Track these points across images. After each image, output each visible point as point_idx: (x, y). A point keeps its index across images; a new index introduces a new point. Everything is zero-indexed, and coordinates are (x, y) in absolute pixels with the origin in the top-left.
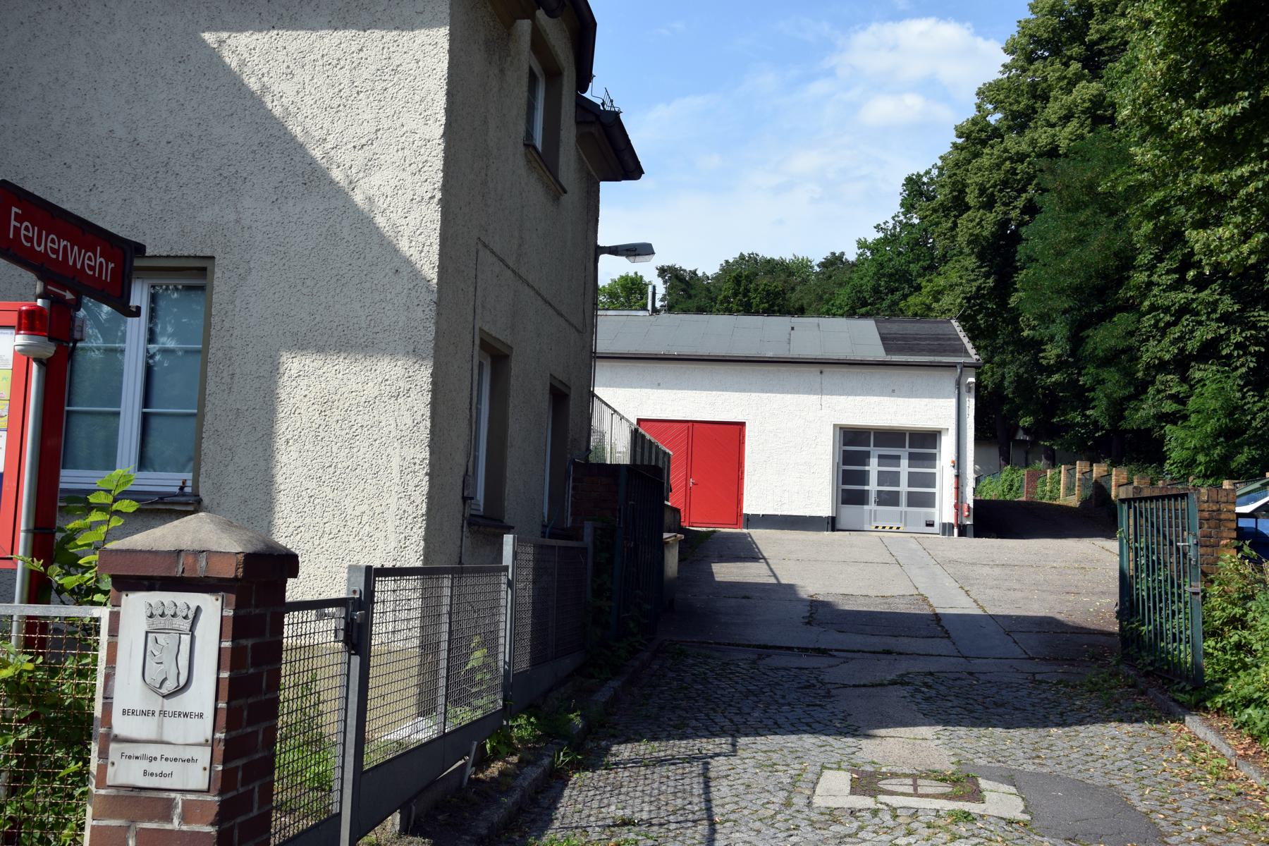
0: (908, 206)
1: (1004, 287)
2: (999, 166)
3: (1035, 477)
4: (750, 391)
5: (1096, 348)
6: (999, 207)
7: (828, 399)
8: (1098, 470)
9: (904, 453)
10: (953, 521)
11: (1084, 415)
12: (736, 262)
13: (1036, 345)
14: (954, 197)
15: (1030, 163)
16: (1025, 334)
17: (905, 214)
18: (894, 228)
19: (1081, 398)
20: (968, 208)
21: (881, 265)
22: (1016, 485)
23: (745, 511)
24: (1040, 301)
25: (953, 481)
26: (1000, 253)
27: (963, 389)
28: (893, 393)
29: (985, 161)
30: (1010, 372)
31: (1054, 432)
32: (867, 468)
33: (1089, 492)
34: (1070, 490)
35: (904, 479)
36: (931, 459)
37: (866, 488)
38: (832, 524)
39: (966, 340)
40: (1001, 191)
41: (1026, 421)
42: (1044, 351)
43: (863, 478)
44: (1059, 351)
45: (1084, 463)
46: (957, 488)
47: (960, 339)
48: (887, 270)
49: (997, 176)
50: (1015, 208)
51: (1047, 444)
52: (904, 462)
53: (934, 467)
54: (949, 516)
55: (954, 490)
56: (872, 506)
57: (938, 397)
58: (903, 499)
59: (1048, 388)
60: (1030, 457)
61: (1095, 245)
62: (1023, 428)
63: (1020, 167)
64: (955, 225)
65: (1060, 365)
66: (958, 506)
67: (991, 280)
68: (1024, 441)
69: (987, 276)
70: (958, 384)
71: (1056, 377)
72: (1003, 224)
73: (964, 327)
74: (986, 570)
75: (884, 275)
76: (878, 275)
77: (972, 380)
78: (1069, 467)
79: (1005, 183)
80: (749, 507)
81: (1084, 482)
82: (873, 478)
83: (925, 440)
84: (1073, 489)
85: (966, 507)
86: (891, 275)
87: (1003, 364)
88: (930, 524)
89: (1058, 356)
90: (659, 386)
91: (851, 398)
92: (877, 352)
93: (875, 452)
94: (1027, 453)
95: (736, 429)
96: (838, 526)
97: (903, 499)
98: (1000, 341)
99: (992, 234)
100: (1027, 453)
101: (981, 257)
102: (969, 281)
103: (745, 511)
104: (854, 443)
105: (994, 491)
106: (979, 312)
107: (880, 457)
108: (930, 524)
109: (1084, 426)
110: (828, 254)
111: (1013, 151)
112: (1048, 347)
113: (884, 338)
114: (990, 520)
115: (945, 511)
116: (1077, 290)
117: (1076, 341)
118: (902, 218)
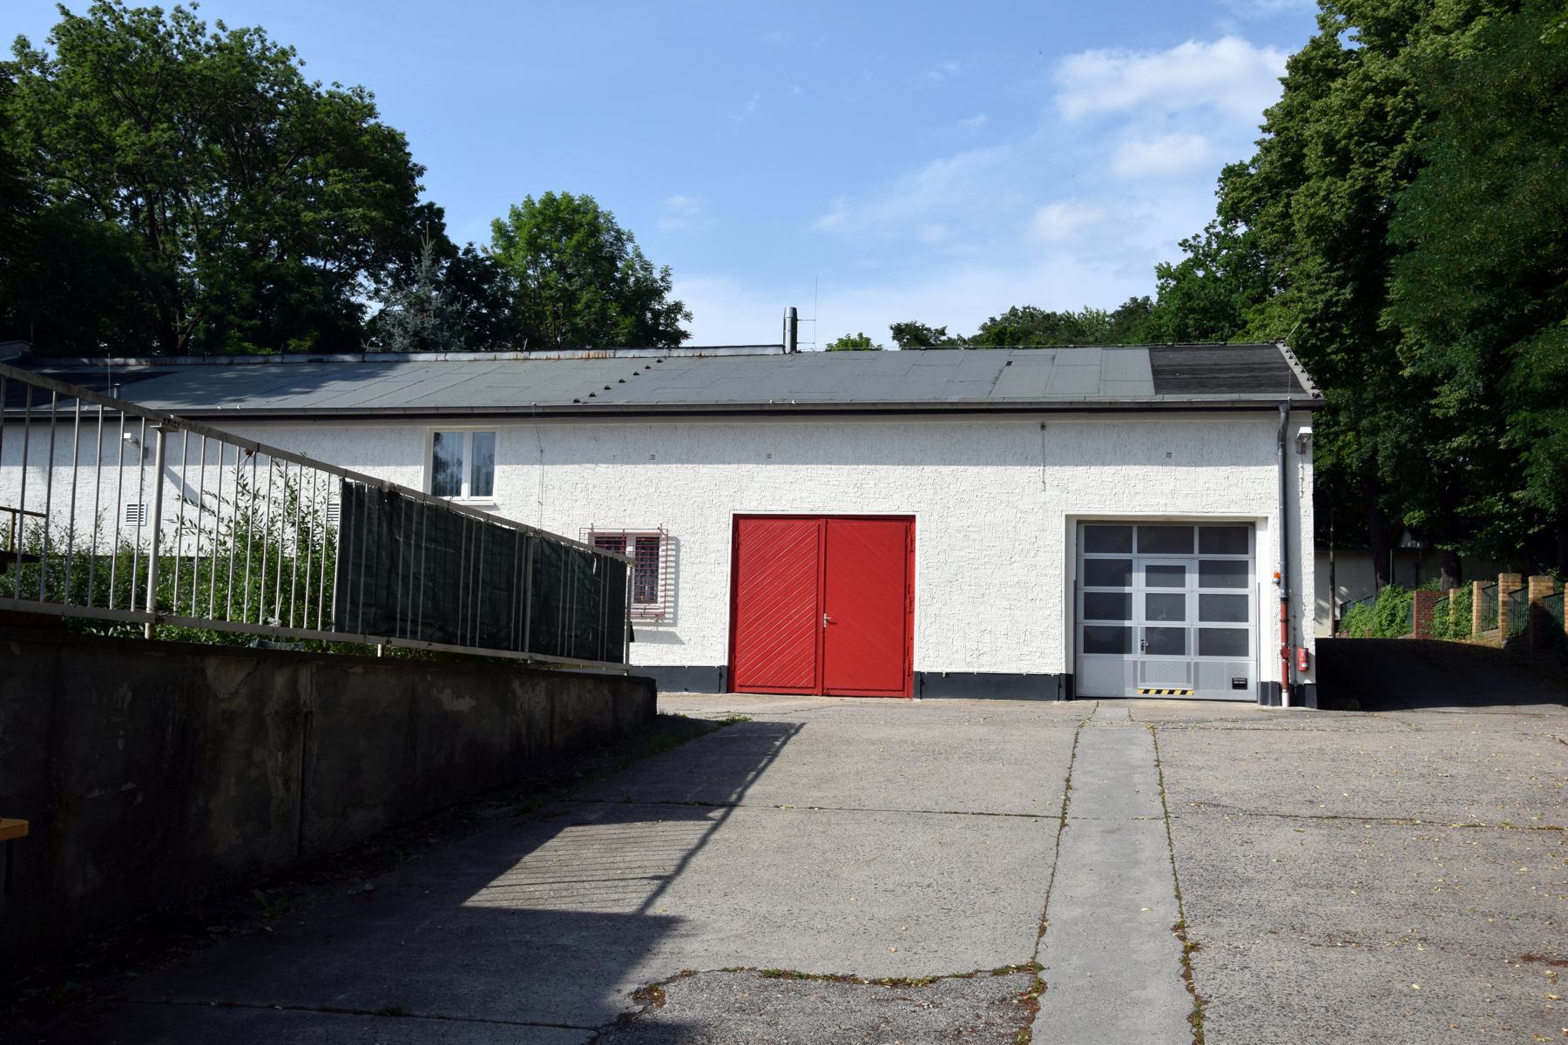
0: (1230, 212)
1: (1371, 296)
2: (1354, 105)
3: (1429, 602)
4: (921, 462)
5: (1529, 375)
6: (1357, 170)
7: (1055, 473)
8: (1537, 587)
9: (1191, 562)
10: (1279, 679)
11: (1509, 500)
12: (1005, 319)
13: (1426, 386)
14: (1285, 165)
15: (1407, 95)
16: (1407, 373)
17: (1223, 224)
18: (1209, 243)
19: (1504, 470)
20: (1308, 178)
21: (1188, 296)
22: (1401, 614)
23: (916, 668)
24: (1427, 300)
25: (1277, 608)
26: (1361, 247)
27: (1293, 448)
28: (1168, 458)
29: (1335, 100)
30: (1386, 442)
31: (1457, 529)
32: (1127, 590)
33: (1521, 625)
34: (1488, 620)
35: (1192, 607)
36: (1240, 572)
37: (1127, 623)
38: (1067, 687)
39: (1298, 370)
40: (1359, 144)
41: (1413, 517)
42: (1436, 395)
43: (1121, 606)
44: (1463, 393)
45: (1511, 577)
46: (1286, 621)
47: (1289, 368)
48: (1195, 303)
49: (1353, 119)
50: (1383, 169)
51: (1448, 548)
52: (1192, 579)
53: (1245, 585)
54: (1272, 671)
55: (1279, 626)
56: (1137, 656)
57: (1248, 464)
58: (1192, 642)
59: (1443, 465)
60: (1423, 573)
61: (1522, 194)
62: (1411, 529)
63: (1390, 101)
64: (1288, 205)
65: (1466, 418)
66: (1288, 653)
67: (1348, 289)
68: (1412, 550)
69: (1341, 283)
70: (1283, 440)
71: (1458, 441)
72: (1365, 197)
73: (1305, 365)
74: (1280, 841)
75: (1192, 310)
76: (1184, 311)
77: (1307, 430)
78: (1486, 583)
79: (1366, 134)
80: (925, 661)
81: (1512, 609)
82: (1138, 606)
83: (1231, 538)
84: (1494, 619)
85: (1302, 654)
86: (1204, 310)
87: (1374, 431)
88: (1240, 685)
89: (1462, 402)
90: (769, 459)
91: (1094, 469)
92: (1145, 391)
93: (1141, 562)
94: (1417, 567)
95: (898, 531)
96: (1081, 691)
97: (1192, 642)
98: (1368, 395)
99: (1348, 217)
100: (1417, 567)
101: (1331, 254)
102: (1312, 294)
103: (916, 668)
104: (1102, 546)
105: (1365, 624)
106: (1330, 341)
107: (1150, 570)
108: (1240, 685)
109: (1509, 517)
110: (1127, 300)
111: (1378, 79)
112: (1446, 388)
113: (1156, 372)
114: (1346, 678)
115: (1266, 663)
116: (1493, 279)
117: (1495, 364)
118: (1219, 229)
